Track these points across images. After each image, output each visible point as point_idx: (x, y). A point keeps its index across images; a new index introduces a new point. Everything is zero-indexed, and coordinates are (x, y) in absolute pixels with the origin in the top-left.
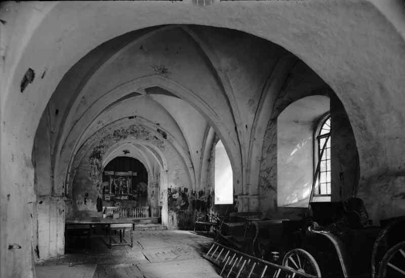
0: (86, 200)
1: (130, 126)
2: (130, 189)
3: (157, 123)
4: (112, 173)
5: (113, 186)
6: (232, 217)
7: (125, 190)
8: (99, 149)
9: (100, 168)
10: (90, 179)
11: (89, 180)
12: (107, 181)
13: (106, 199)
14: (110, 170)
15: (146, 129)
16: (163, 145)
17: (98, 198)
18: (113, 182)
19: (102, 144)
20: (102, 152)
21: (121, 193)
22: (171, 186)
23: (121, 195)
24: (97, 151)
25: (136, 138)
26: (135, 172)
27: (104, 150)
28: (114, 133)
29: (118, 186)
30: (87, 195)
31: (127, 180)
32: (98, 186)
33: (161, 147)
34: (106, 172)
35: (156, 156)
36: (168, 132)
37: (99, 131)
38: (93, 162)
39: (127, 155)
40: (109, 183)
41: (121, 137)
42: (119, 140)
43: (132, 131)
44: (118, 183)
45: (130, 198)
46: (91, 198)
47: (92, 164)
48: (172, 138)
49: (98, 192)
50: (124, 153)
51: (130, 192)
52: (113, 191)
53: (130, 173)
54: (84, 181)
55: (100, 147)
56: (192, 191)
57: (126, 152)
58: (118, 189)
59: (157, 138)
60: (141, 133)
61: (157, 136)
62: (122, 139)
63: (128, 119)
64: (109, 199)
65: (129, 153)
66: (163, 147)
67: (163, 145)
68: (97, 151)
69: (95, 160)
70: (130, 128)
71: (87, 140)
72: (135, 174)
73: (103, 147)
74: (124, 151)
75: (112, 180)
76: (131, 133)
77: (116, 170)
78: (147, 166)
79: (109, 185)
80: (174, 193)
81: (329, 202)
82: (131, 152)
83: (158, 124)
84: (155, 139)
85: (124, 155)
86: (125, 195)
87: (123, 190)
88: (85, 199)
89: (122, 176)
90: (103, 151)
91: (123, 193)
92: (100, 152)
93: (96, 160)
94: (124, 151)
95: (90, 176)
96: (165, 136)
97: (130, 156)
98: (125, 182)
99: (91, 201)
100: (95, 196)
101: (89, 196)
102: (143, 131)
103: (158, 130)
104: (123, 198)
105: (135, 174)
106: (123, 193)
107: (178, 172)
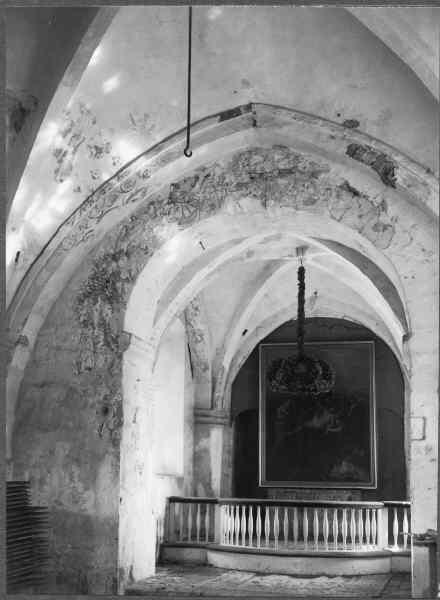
1: (238, 157)
3: (347, 116)
8: (114, 264)
9: (115, 341)
12: (266, 492)
15: (307, 160)
16: (385, 219)
24: (104, 271)
25: (264, 205)
36: (398, 152)
38: (90, 315)
47: (85, 324)
48: (423, 176)
56: (41, 541)
67: (385, 219)
68: (104, 271)
71: (335, 576)
73: (128, 254)
83: (352, 124)
84: (347, 197)
90: (130, 271)
92: (116, 274)
96: (387, 176)
103: (354, 151)
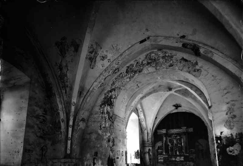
0: (95, 161)
2: (186, 148)
4: (164, 131)
5: (167, 146)
6: (64, 78)
7: (180, 150)
9: (111, 118)
10: (100, 132)
11: (99, 134)
13: (159, 161)
14: (161, 129)
16: (197, 67)
17: (109, 158)
18: (166, 141)
19: (113, 87)
20: (113, 97)
21: (176, 153)
22: (221, 133)
23: (176, 156)
24: (108, 96)
26: (190, 127)
27: (116, 94)
28: (127, 70)
29: (172, 145)
30: (96, 154)
31: (181, 138)
32: (109, 141)
33: (195, 71)
34: (158, 131)
35: (195, 91)
37: (105, 70)
38: (103, 110)
39: (180, 110)
40: (163, 143)
41: (135, 72)
42: (133, 77)
43: (150, 61)
44: (171, 141)
45: (186, 158)
46: (101, 159)
47: (102, 113)
49: (110, 149)
50: (174, 108)
51: (186, 152)
52: (167, 151)
53: (183, 129)
54: (94, 136)
55: (111, 91)
57: (177, 106)
58: (172, 149)
59: (186, 60)
60: (161, 60)
61: (185, 58)
62: (137, 75)
63: (139, 45)
64: (162, 160)
65: (180, 106)
66: (198, 70)
67: (197, 67)
69: (105, 109)
70: (146, 58)
72: (191, 130)
74: (174, 106)
75: (164, 139)
76: (148, 64)
77: (168, 129)
78: (204, 118)
79: (163, 144)
80: (228, 146)
81: (139, 164)
82: (183, 105)
85: (176, 111)
86: (180, 156)
87: (177, 149)
88: (94, 160)
89: (176, 134)
91: (178, 153)
92: (111, 97)
93: (107, 108)
94: (174, 106)
95: (101, 129)
97: (184, 111)
98: (180, 140)
99: (100, 162)
100: (105, 155)
101: (99, 155)
102: (163, 57)
104: (178, 159)
105: (191, 130)
106: (178, 153)
107: (234, 105)
